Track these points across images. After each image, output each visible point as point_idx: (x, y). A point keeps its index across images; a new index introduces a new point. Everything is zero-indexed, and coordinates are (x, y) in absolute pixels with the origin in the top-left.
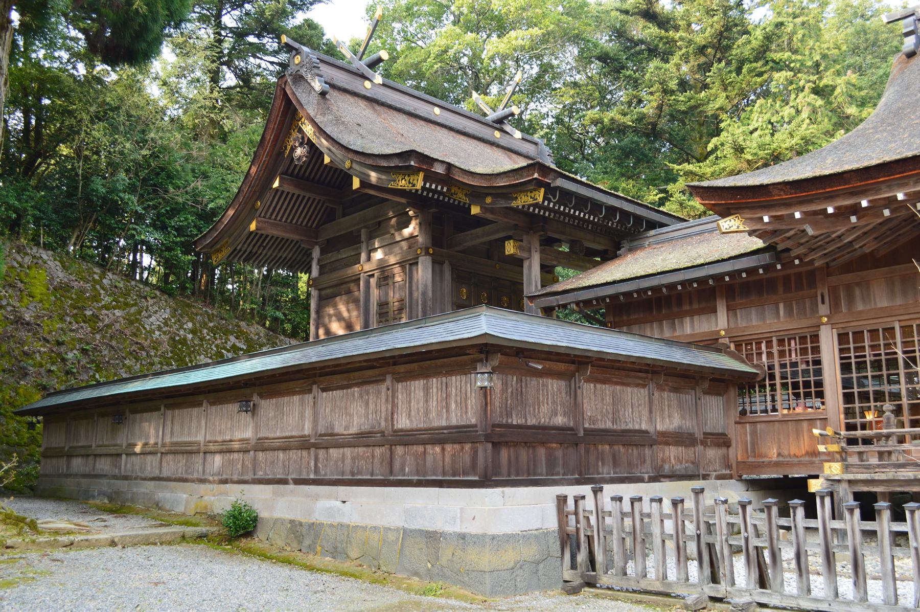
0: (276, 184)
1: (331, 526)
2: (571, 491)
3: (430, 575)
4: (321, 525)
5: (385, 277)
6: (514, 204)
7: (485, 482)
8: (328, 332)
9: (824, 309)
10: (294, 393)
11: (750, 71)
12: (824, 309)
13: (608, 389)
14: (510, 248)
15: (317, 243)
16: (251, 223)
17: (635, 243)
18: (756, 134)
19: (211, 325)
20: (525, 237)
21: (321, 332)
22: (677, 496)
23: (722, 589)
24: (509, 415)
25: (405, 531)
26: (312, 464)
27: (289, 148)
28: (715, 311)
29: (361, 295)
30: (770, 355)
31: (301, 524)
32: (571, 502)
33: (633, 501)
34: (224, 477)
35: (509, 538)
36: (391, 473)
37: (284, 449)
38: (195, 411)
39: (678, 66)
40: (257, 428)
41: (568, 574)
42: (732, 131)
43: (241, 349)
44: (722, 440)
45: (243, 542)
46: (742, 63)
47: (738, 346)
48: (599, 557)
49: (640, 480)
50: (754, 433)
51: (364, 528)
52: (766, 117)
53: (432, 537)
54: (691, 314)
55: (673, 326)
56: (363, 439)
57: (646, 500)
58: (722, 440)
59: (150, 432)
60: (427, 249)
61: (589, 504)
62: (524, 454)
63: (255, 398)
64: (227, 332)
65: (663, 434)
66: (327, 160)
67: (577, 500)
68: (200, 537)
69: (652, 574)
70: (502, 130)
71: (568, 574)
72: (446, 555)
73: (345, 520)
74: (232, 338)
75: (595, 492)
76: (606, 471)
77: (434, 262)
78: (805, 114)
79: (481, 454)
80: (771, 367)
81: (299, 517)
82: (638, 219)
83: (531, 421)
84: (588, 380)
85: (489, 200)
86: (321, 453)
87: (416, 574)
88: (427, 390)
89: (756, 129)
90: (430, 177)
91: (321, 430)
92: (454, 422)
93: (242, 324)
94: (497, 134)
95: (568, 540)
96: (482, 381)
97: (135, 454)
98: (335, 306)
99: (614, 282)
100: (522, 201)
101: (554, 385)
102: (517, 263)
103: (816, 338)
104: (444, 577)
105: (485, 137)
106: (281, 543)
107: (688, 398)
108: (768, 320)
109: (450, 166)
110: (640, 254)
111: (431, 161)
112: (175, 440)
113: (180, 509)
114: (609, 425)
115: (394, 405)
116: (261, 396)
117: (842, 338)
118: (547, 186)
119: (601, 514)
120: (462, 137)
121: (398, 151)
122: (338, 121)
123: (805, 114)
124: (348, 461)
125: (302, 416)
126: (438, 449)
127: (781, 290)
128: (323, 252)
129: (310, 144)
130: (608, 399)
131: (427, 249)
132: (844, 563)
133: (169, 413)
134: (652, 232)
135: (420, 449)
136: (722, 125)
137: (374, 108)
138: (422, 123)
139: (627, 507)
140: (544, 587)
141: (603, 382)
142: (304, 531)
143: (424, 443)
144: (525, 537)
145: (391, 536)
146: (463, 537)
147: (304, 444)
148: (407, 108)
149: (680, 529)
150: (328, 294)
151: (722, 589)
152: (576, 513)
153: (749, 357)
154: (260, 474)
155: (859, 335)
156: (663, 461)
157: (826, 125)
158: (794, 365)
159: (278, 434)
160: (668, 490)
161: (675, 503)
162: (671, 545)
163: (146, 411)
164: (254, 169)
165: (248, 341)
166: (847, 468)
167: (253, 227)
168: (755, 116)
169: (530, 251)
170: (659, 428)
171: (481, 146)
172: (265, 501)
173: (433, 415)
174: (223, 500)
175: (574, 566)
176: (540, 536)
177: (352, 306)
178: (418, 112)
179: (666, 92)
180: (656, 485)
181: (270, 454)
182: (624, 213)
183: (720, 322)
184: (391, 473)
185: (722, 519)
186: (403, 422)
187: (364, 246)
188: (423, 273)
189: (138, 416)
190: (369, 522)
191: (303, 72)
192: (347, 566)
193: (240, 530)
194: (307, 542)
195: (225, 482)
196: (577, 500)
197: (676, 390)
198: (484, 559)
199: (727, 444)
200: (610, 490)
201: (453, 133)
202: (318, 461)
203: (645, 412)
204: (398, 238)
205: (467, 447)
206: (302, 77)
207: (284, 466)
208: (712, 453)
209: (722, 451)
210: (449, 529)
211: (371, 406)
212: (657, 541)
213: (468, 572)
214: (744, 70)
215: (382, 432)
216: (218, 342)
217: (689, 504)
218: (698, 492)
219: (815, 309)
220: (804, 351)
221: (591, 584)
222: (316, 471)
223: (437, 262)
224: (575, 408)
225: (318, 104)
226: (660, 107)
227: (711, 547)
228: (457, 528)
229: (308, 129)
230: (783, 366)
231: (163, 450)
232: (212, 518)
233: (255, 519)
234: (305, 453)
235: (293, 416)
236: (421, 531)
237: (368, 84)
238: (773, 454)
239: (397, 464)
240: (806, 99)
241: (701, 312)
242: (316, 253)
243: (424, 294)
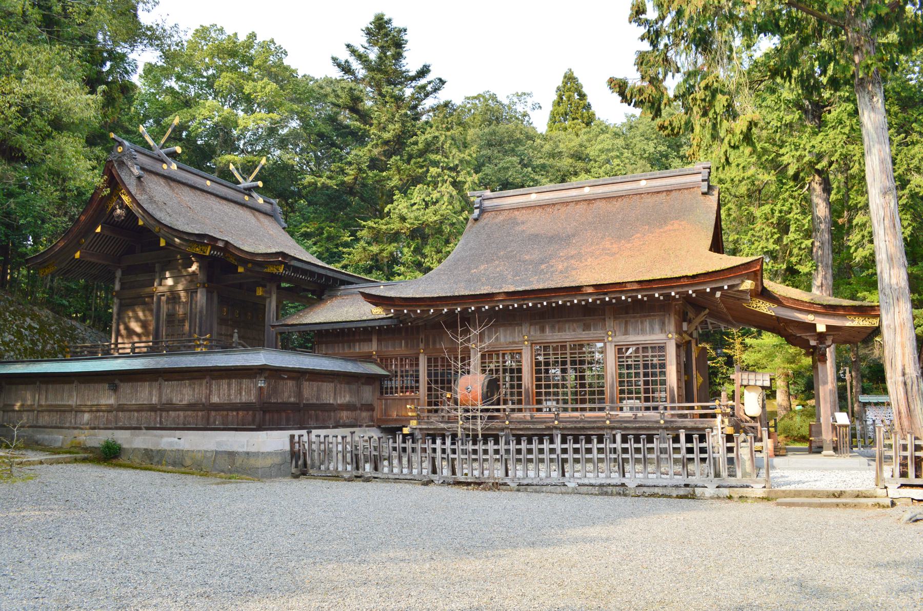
0: (99, 230)
1: (172, 451)
2: (297, 433)
3: (230, 472)
4: (165, 451)
5: (173, 297)
6: (265, 270)
7: (259, 428)
8: (127, 328)
9: (422, 346)
10: (146, 381)
11: (415, 163)
12: (422, 346)
13: (315, 384)
14: (260, 292)
15: (119, 267)
16: (76, 252)
17: (332, 293)
18: (415, 207)
19: (12, 309)
20: (268, 285)
21: (122, 327)
22: (344, 435)
23: (361, 472)
24: (270, 398)
25: (216, 452)
26: (158, 419)
27: (110, 208)
28: (371, 341)
29: (154, 306)
30: (396, 365)
31: (151, 450)
32: (296, 439)
33: (325, 437)
34: (92, 425)
35: (269, 453)
36: (208, 424)
37: (138, 411)
38: (67, 387)
39: (370, 151)
40: (118, 399)
41: (294, 470)
42: (400, 205)
43: (36, 328)
44: (370, 408)
45: (114, 461)
46: (410, 157)
47: (381, 360)
48: (309, 462)
49: (328, 428)
50: (386, 404)
51: (193, 451)
52: (423, 196)
53: (232, 454)
54: (360, 341)
55: (350, 348)
56: (191, 407)
57: (331, 437)
58: (370, 408)
59: (29, 397)
60: (204, 284)
61: (305, 438)
62: (276, 416)
63: (117, 382)
64: (24, 315)
65: (340, 405)
66: (141, 223)
67: (300, 436)
68: (84, 460)
69: (331, 468)
70: (250, 195)
71: (294, 470)
72: (238, 462)
73: (181, 448)
74: (28, 319)
75: (309, 433)
76: (312, 424)
77: (208, 292)
78: (445, 199)
79: (257, 416)
80: (396, 372)
81: (150, 447)
82: (335, 279)
83: (279, 401)
84: (306, 380)
85: (250, 265)
86: (164, 414)
87: (222, 471)
88: (229, 385)
89: (415, 204)
90: (215, 248)
91: (164, 401)
92: (244, 401)
93: (36, 308)
94: (247, 198)
95: (294, 454)
96: (261, 384)
97: (14, 411)
98: (134, 311)
99: (320, 323)
100: (271, 269)
101: (290, 383)
102: (263, 298)
103: (417, 359)
104: (238, 472)
105: (239, 200)
106: (137, 461)
107: (354, 387)
108: (398, 349)
109: (227, 243)
110: (336, 302)
111: (216, 240)
112: (49, 403)
113: (59, 444)
114: (315, 401)
115: (211, 391)
116: (121, 381)
117: (429, 360)
118: (286, 264)
119: (310, 443)
120: (225, 202)
121: (197, 232)
122: (151, 199)
123: (445, 199)
124: (182, 418)
125: (150, 393)
126: (235, 413)
127: (403, 334)
128: (123, 273)
129: (127, 207)
130: (315, 389)
131: (204, 284)
132: (405, 460)
133: (44, 387)
134: (342, 287)
135: (225, 413)
136: (395, 197)
137: (170, 186)
138: (199, 192)
139: (322, 439)
140: (284, 476)
141: (313, 381)
142: (154, 454)
143: (227, 410)
144: (276, 453)
145: (208, 455)
146: (248, 453)
147: (152, 408)
148: (190, 182)
149: (345, 448)
150: (127, 305)
151: (361, 472)
152: (299, 442)
153: (386, 366)
154: (120, 424)
155: (436, 360)
156: (340, 418)
157: (458, 206)
158: (407, 371)
159: (133, 402)
160: (340, 432)
161: (343, 438)
162: (340, 456)
163: (22, 384)
164: (83, 218)
165: (40, 322)
166: (419, 423)
167: (77, 255)
168: (415, 194)
169: (270, 293)
170: (339, 402)
171: (237, 207)
172: (122, 438)
173: (232, 397)
174: (100, 438)
175: (296, 466)
176: (282, 453)
177: (147, 313)
178: (197, 185)
179: (360, 170)
180: (336, 430)
181: (127, 414)
182: (326, 276)
183: (373, 347)
184: (208, 424)
185: (361, 444)
186: (215, 399)
187: (157, 275)
188: (201, 297)
189: (14, 387)
190: (195, 448)
191: (125, 159)
192: (187, 470)
193: (110, 455)
194: (156, 460)
195: (94, 428)
196: (300, 436)
197: (348, 383)
198: (260, 463)
199: (373, 410)
200: (315, 432)
201: (218, 199)
202: (162, 417)
203: (332, 395)
204: (185, 274)
205: (250, 413)
206: (123, 163)
207: (138, 420)
208: (364, 414)
209: (369, 413)
210: (240, 450)
211: (197, 391)
212: (334, 453)
213: (250, 469)
214: (412, 162)
215: (203, 404)
216: (18, 322)
217: (349, 439)
218: (352, 433)
219: (418, 345)
220: (411, 365)
221: (304, 473)
222: (161, 423)
223: (209, 292)
224: (299, 394)
225: (137, 186)
226: (356, 179)
227: (357, 455)
228: (245, 450)
229: (126, 199)
230: (402, 372)
231: (40, 409)
232: (86, 450)
233: (120, 448)
234: (153, 414)
235: (147, 394)
236: (225, 452)
237: (165, 166)
238: (394, 415)
239: (212, 420)
240: (447, 189)
241: (364, 341)
242: (119, 274)
243: (201, 312)
